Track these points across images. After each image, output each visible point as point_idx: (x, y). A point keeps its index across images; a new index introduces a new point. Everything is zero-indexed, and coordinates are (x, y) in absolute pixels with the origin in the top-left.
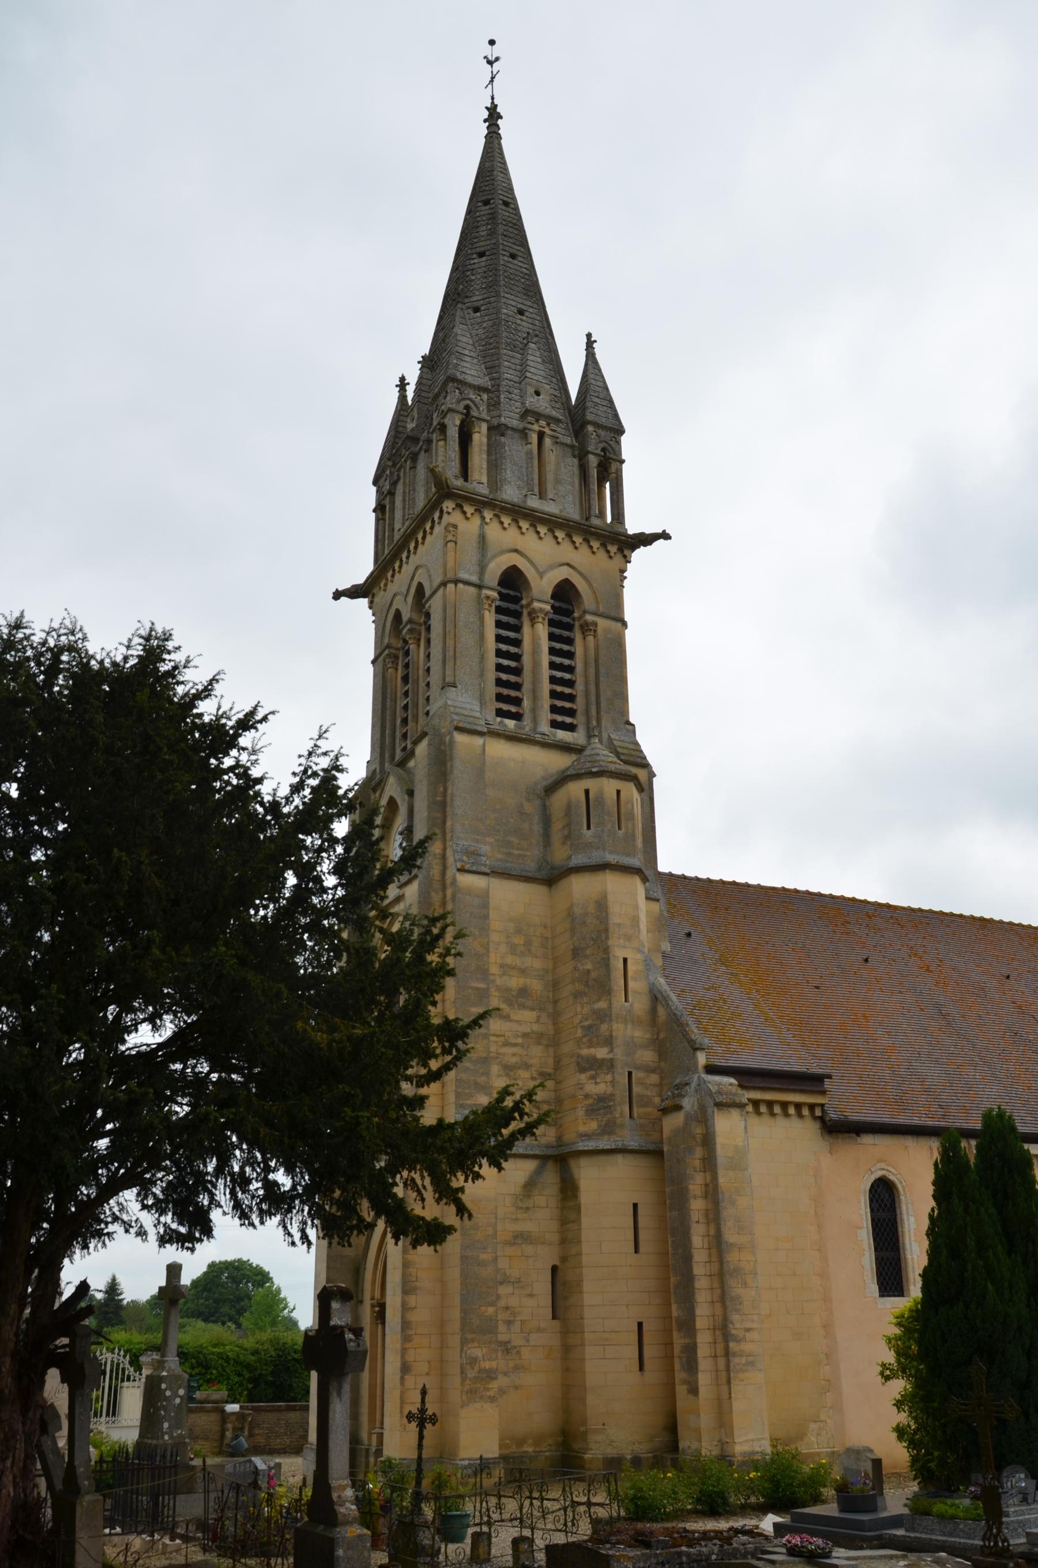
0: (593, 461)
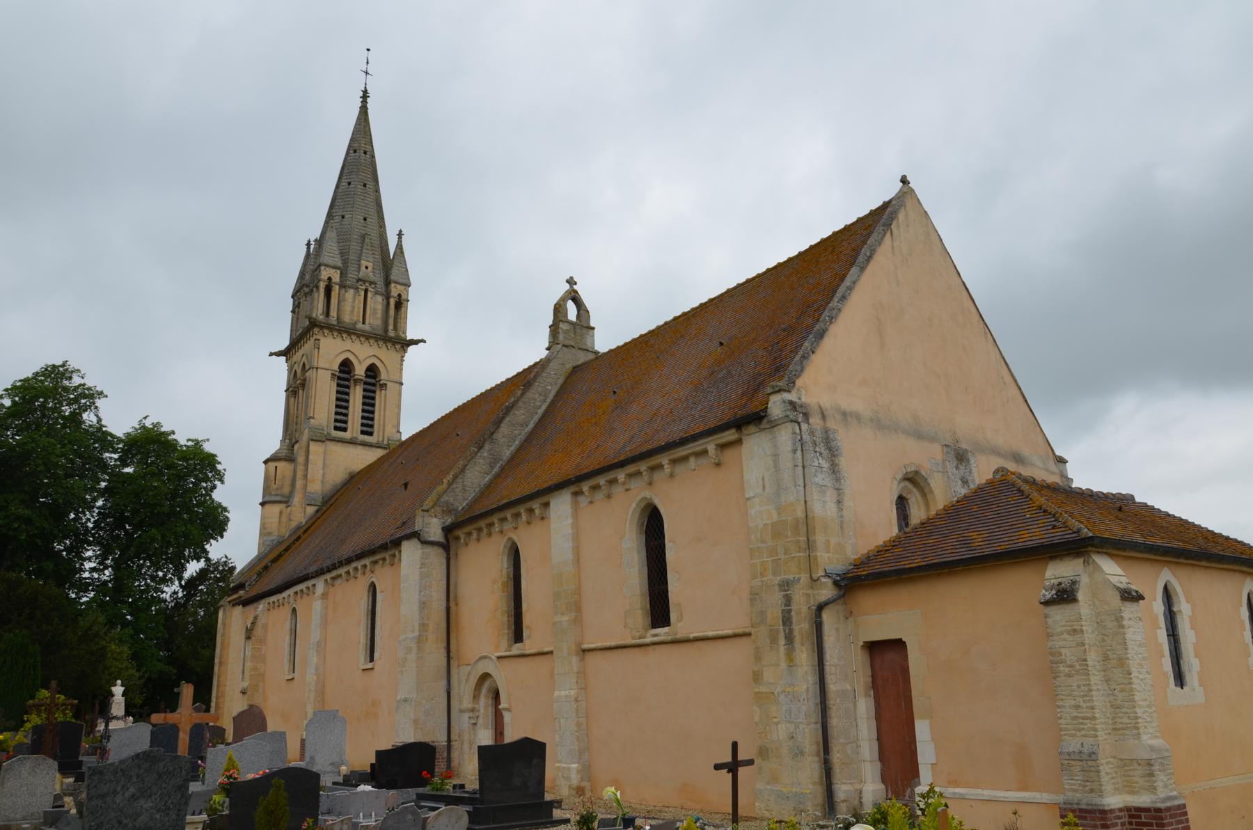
0: (392, 302)
